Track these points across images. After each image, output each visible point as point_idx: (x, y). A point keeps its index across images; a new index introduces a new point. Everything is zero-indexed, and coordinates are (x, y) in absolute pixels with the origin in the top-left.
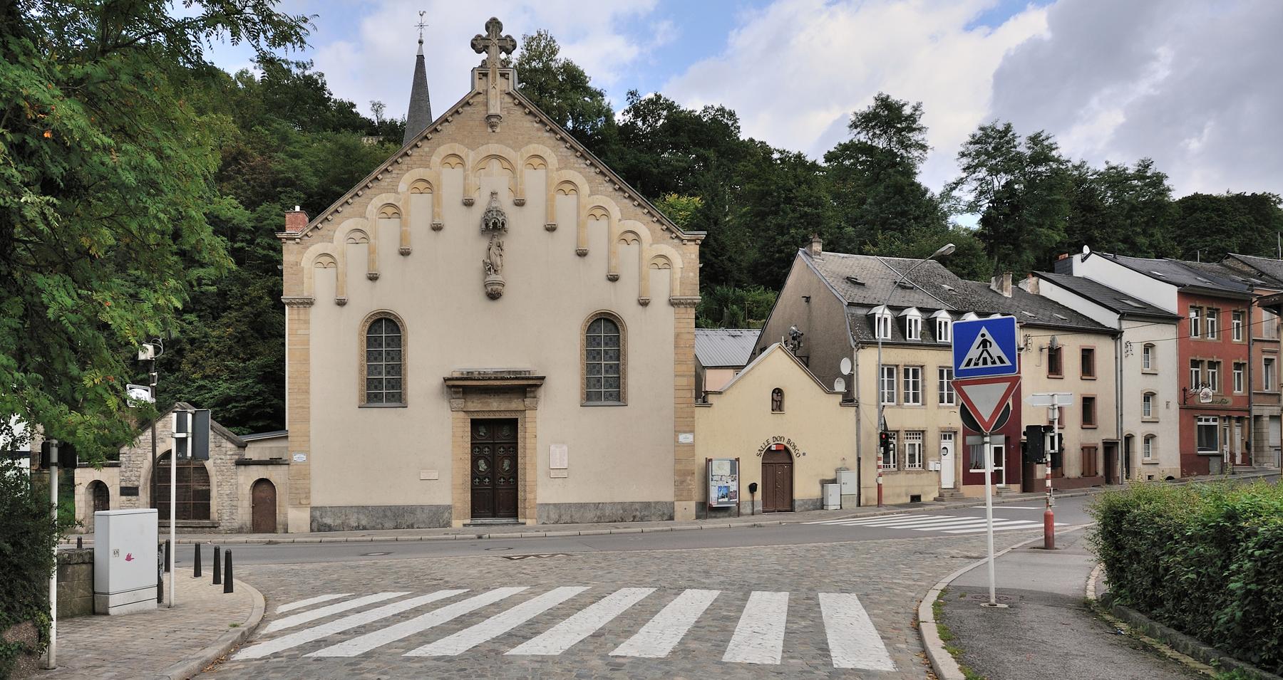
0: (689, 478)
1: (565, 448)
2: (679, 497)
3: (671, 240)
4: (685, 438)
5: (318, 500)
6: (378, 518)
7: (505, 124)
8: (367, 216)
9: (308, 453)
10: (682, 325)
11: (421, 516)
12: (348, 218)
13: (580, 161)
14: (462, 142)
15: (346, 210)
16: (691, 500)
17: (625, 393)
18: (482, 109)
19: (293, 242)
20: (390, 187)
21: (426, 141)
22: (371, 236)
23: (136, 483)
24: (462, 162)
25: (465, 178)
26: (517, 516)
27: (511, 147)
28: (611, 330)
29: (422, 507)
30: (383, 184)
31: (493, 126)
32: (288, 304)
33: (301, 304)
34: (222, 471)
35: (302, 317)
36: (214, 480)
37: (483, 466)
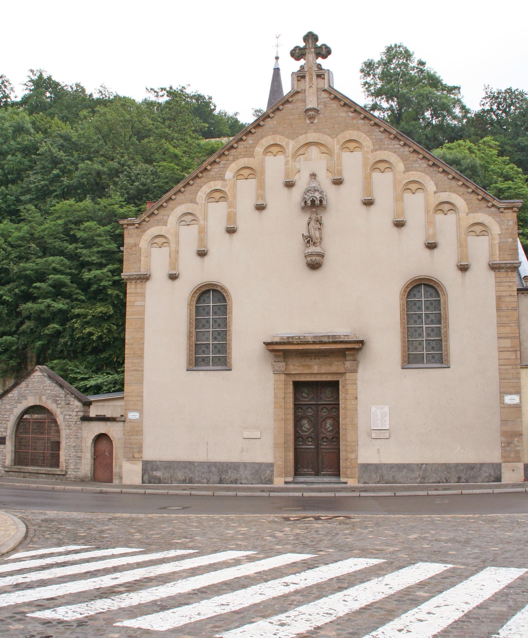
0: (516, 439)
1: (386, 409)
2: (506, 458)
3: (488, 209)
4: (511, 399)
5: (149, 455)
6: (203, 473)
7: (321, 116)
8: (197, 201)
9: (141, 412)
10: (502, 288)
11: (245, 473)
12: (179, 204)
13: (395, 142)
14: (283, 134)
15: (180, 197)
16: (519, 462)
17: (447, 355)
19: (134, 227)
20: (218, 175)
21: (250, 135)
22: (201, 218)
23: (4, 434)
26: (339, 475)
27: (329, 135)
28: (431, 295)
29: (245, 465)
30: (212, 173)
31: (311, 118)
34: (70, 426)
35: (139, 291)
36: (64, 433)
37: (306, 425)
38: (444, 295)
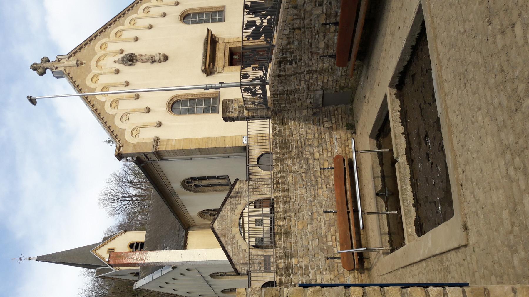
17: (219, 7)
18: (73, 68)
24: (97, 75)
25: (105, 74)
32: (156, 149)
33: (157, 143)
38: (190, 10)
